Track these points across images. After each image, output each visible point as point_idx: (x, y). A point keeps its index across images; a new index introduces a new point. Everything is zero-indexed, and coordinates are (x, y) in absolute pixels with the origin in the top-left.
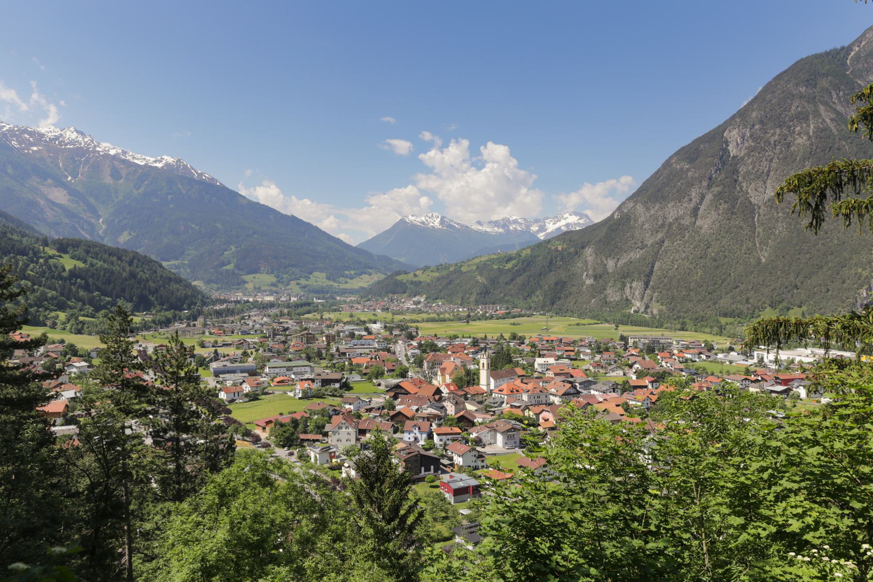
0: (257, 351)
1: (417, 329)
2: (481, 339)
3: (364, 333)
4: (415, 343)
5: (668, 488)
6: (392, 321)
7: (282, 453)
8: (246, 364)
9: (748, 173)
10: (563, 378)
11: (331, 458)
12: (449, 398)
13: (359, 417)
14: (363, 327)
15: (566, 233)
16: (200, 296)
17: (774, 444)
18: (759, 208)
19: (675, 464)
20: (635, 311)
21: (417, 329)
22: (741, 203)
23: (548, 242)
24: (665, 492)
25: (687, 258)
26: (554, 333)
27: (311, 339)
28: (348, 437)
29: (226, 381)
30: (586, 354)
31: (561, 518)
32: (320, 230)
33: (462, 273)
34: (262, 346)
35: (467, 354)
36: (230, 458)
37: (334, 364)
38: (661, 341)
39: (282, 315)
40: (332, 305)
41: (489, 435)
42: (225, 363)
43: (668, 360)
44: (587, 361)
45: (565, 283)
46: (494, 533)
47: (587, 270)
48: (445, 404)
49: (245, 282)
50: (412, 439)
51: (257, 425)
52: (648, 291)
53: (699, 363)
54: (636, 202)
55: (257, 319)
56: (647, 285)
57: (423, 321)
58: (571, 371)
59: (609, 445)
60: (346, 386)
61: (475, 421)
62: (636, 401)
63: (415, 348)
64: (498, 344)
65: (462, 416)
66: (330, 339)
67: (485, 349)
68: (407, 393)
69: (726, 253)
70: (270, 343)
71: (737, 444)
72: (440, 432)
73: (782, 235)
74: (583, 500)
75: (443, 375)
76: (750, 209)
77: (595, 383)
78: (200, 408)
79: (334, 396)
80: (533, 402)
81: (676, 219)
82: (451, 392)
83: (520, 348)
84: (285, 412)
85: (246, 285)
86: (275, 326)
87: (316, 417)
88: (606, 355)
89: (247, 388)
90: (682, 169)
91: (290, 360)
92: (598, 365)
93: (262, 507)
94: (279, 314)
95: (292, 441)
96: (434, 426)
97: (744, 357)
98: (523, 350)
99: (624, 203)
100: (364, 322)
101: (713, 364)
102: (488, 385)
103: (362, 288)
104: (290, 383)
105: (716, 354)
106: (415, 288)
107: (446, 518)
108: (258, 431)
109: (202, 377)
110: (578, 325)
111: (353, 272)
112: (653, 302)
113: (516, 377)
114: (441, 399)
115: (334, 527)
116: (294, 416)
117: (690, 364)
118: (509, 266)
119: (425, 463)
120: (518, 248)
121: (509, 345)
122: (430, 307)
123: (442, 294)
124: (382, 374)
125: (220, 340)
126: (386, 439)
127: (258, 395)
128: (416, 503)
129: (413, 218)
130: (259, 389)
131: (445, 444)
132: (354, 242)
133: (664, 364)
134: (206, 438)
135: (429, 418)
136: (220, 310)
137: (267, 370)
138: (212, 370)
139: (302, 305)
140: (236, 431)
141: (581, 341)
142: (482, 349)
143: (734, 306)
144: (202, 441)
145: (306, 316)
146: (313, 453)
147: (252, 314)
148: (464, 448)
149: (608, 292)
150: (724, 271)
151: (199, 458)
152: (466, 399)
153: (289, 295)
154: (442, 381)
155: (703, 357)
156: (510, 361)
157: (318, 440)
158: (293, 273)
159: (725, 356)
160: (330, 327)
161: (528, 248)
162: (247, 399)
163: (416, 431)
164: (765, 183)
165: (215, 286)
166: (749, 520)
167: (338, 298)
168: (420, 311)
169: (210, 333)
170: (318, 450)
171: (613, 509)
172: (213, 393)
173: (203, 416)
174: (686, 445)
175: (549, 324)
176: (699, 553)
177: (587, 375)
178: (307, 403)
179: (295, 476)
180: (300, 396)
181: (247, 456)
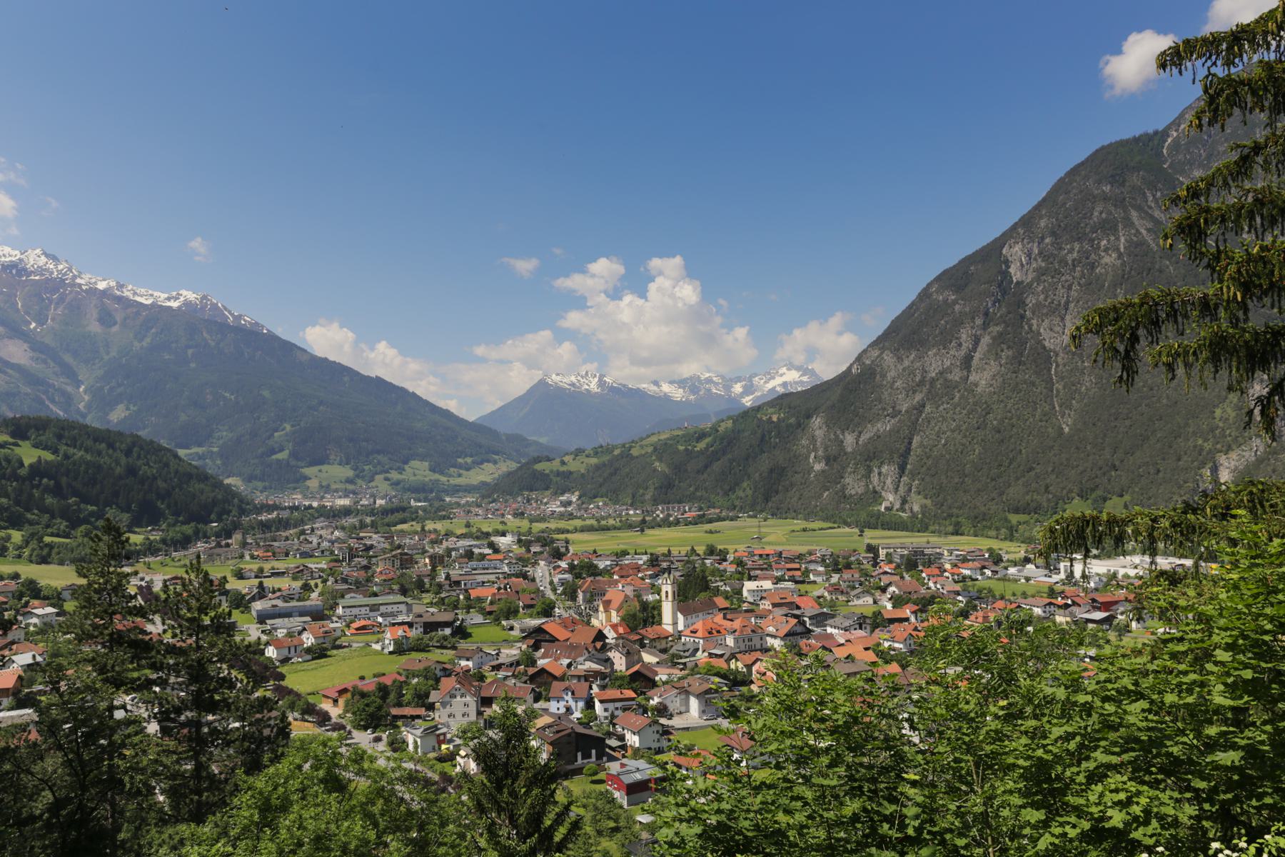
0: (325, 581)
1: (567, 542)
2: (663, 555)
3: (487, 551)
4: (564, 564)
7: (363, 738)
8: (308, 603)
9: (1038, 305)
10: (785, 610)
11: (440, 743)
12: (617, 645)
13: (481, 678)
14: (485, 542)
16: (236, 500)
17: (1082, 698)
18: (1057, 355)
23: (757, 409)
25: (958, 428)
26: (769, 543)
28: (466, 709)
29: (276, 629)
30: (818, 574)
33: (633, 458)
34: (332, 575)
35: (643, 579)
37: (443, 599)
38: (927, 552)
39: (363, 526)
40: (438, 510)
42: (274, 602)
47: (815, 450)
49: (306, 478)
50: (563, 710)
51: (325, 696)
52: (905, 479)
53: (982, 582)
54: (883, 350)
55: (323, 534)
56: (902, 469)
57: (576, 530)
58: (796, 599)
59: (842, 709)
60: (462, 632)
61: (657, 678)
63: (565, 571)
64: (688, 562)
66: (437, 561)
67: (669, 570)
68: (554, 640)
70: (345, 569)
71: (1030, 701)
73: (1091, 393)
74: (809, 795)
75: (606, 611)
76: (1043, 357)
77: (833, 616)
78: (234, 673)
80: (743, 648)
81: (941, 373)
82: (620, 637)
83: (721, 567)
85: (308, 483)
86: (353, 543)
87: (416, 680)
88: (847, 575)
89: (308, 640)
90: (945, 301)
91: (375, 595)
92: (835, 589)
93: (328, 823)
96: (595, 689)
97: (1046, 572)
99: (865, 351)
100: (488, 535)
101: (1001, 583)
102: (675, 624)
103: (484, 483)
105: (1006, 568)
106: (561, 483)
107: (616, 830)
108: (326, 706)
110: (804, 530)
111: (469, 460)
112: (912, 495)
114: (605, 648)
116: (381, 680)
117: (970, 583)
118: (701, 446)
119: (582, 745)
120: (714, 420)
121: (704, 564)
123: (604, 490)
126: (520, 710)
127: (326, 649)
128: (567, 808)
129: (559, 378)
130: (327, 640)
131: (613, 716)
132: (470, 414)
133: (931, 584)
134: (242, 719)
135: (588, 677)
137: (340, 611)
138: (254, 613)
139: (393, 511)
140: (292, 707)
142: (663, 571)
143: (1028, 498)
144: (237, 725)
145: (400, 527)
148: (641, 721)
149: (847, 480)
152: (643, 646)
153: (374, 496)
154: (605, 621)
155: (988, 572)
156: (706, 587)
157: (418, 717)
158: (379, 463)
159: (1019, 571)
161: (729, 418)
162: (309, 657)
163: (569, 697)
164: (1063, 319)
165: (260, 484)
166: (1053, 813)
167: (448, 499)
168: (571, 516)
169: (252, 557)
170: (418, 732)
171: (852, 807)
175: (763, 530)
177: (820, 604)
179: (382, 774)
180: (391, 649)
181: (304, 745)
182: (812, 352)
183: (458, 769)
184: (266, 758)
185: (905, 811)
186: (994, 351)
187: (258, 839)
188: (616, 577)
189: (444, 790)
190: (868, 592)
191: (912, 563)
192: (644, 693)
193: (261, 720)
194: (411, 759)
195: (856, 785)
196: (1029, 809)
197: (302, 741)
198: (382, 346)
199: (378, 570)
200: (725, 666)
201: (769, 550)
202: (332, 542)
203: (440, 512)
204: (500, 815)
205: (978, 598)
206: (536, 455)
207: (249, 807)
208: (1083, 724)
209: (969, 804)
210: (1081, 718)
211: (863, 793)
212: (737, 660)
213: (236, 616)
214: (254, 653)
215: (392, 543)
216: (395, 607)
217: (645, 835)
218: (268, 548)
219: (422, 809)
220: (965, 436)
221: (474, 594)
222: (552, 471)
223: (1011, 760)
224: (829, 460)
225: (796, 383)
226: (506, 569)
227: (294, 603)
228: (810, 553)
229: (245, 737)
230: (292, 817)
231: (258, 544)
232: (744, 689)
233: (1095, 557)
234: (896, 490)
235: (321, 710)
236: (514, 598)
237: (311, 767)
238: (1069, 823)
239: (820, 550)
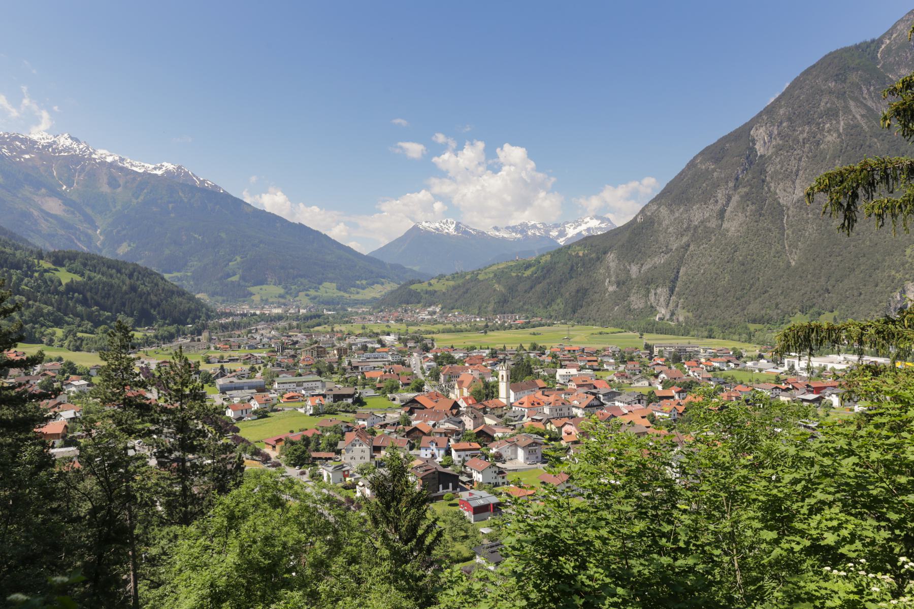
0: (265, 366)
2: (500, 350)
4: (430, 356)
6: (407, 333)
9: (776, 172)
10: (585, 389)
11: (345, 476)
12: (467, 412)
13: (373, 433)
14: (376, 339)
17: (807, 454)
18: (788, 209)
20: (660, 319)
21: (433, 340)
23: (568, 247)
24: (694, 506)
26: (575, 342)
27: (321, 352)
28: (363, 454)
29: (233, 398)
30: (609, 364)
33: (479, 281)
35: (485, 366)
37: (346, 379)
38: (688, 349)
39: (291, 328)
40: (343, 317)
42: (231, 379)
43: (695, 369)
44: (611, 371)
45: (586, 290)
47: (609, 276)
49: (252, 294)
50: (429, 456)
52: (673, 298)
53: (727, 372)
54: (660, 205)
55: (265, 333)
56: (672, 291)
57: (439, 332)
58: (594, 382)
59: (635, 459)
60: (359, 402)
62: (662, 412)
63: (431, 360)
64: (518, 355)
66: (342, 352)
67: (504, 360)
68: (423, 408)
69: (755, 257)
70: (279, 357)
74: (610, 517)
75: (460, 388)
76: (778, 211)
77: (619, 394)
78: (206, 427)
79: (346, 412)
80: (555, 415)
82: (469, 406)
83: (541, 359)
85: (253, 297)
87: (328, 434)
88: (630, 365)
89: (255, 405)
90: (707, 170)
91: (300, 375)
92: (622, 375)
95: (304, 459)
96: (452, 442)
97: (775, 365)
98: (544, 361)
99: (647, 206)
100: (377, 334)
102: (508, 398)
103: (374, 298)
104: (301, 399)
105: (745, 362)
106: (430, 298)
107: (466, 537)
108: (268, 450)
109: (207, 394)
111: (364, 282)
112: (679, 309)
114: (458, 414)
115: (349, 549)
116: (305, 433)
117: (718, 372)
118: (528, 273)
119: (443, 480)
120: (537, 255)
121: (529, 356)
124: (397, 388)
125: (226, 355)
126: (402, 456)
127: (267, 412)
128: (434, 523)
129: (427, 225)
131: (464, 461)
132: (365, 250)
133: (691, 373)
134: (213, 458)
135: (447, 434)
137: (276, 386)
138: (218, 387)
139: (311, 317)
140: (245, 450)
141: (605, 350)
143: (763, 312)
144: (209, 461)
145: (316, 328)
146: (326, 472)
148: (484, 464)
149: (632, 298)
150: (752, 275)
151: (206, 479)
152: (485, 413)
153: (298, 307)
154: (460, 395)
155: (732, 365)
156: (530, 373)
157: (330, 459)
158: (302, 284)
161: (548, 253)
162: (256, 417)
163: (434, 447)
164: (794, 183)
165: (220, 298)
166: (782, 535)
167: (349, 309)
168: (435, 322)
169: (216, 348)
170: (330, 469)
173: (210, 435)
174: (716, 457)
175: (571, 333)
177: (610, 386)
178: (318, 420)
183: (358, 494)
188: (467, 365)
189: (349, 509)
201: (575, 347)
206: (411, 279)
208: (807, 472)
220: (718, 268)
230: (249, 523)
234: (667, 305)
236: (395, 378)
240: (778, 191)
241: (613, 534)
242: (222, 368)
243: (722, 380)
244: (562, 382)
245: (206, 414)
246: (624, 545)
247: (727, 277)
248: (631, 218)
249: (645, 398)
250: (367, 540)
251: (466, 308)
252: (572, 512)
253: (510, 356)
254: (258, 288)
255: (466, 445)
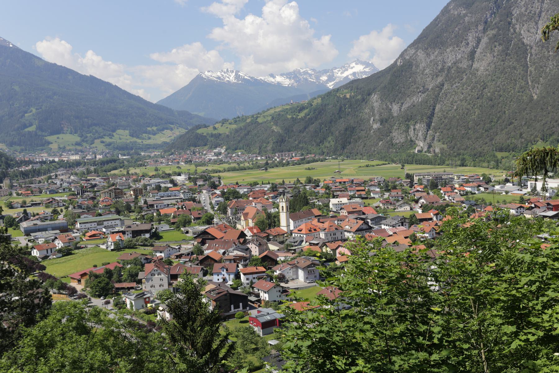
0: (67, 208)
1: (220, 178)
2: (280, 184)
3: (170, 185)
4: (218, 192)
5: (449, 306)
6: (196, 173)
7: (98, 302)
8: (56, 222)
9: (521, 15)
10: (356, 216)
11: (146, 303)
12: (253, 240)
13: (170, 263)
14: (168, 180)
15: (353, 82)
16: (3, 158)
17: (540, 260)
18: (531, 48)
19: (455, 283)
20: (419, 151)
21: (220, 178)
22: (514, 44)
23: (337, 90)
24: (447, 309)
25: (465, 99)
26: (346, 175)
27: (119, 193)
28: (161, 282)
29: (37, 239)
30: (376, 193)
31: (354, 338)
32: (120, 89)
33: (259, 124)
34: (72, 203)
35: (267, 199)
36: (46, 312)
37: (143, 216)
38: (444, 177)
39: (89, 172)
40: (137, 160)
41: (291, 271)
42: (35, 222)
43: (449, 194)
44: (377, 199)
45: (354, 128)
46: (294, 355)
47: (374, 115)
48: (249, 246)
49: (49, 143)
50: (221, 280)
51: (72, 278)
52: (430, 132)
53: (478, 195)
54: (417, 49)
55: (63, 178)
56: (429, 126)
57: (225, 171)
58: (363, 209)
59: (396, 270)
60: (156, 236)
61: (278, 259)
62: (424, 232)
63: (219, 196)
64: (295, 188)
65: (266, 256)
66: (138, 193)
67: (283, 193)
68: (214, 238)
69: (501, 93)
70: (79, 200)
71: (508, 263)
72: (246, 272)
73: (553, 73)
74: (374, 321)
75: (246, 219)
76: (522, 50)
77: (385, 218)
78: (12, 266)
79: (145, 245)
80: (330, 239)
81: (455, 63)
82: (254, 235)
83: (316, 190)
84: (99, 263)
85: (51, 146)
86: (83, 183)
87: (129, 266)
88: (394, 193)
89: (59, 244)
90: (459, 15)
91: (100, 215)
92: (387, 202)
93: (80, 353)
94: (85, 171)
95: (108, 290)
96: (241, 267)
97: (519, 188)
98: (318, 193)
99: (406, 50)
100: (169, 175)
101: (491, 195)
102: (288, 226)
103: (165, 143)
104: (102, 236)
105: (494, 186)
106: (215, 141)
107: (256, 349)
108: (74, 284)
109: (12, 237)
110: (367, 166)
111: (155, 128)
112: (435, 142)
113: (313, 217)
114: (245, 242)
115: (151, 365)
116: (108, 267)
117: (470, 196)
118: (302, 115)
119: (234, 301)
120: (309, 98)
121: (305, 189)
122: (231, 158)
123: (241, 145)
124: (189, 222)
125: (28, 200)
126: (195, 281)
127: (71, 250)
128: (226, 338)
129: (210, 74)
130: (71, 244)
131: (252, 283)
132: (154, 99)
133: (446, 197)
134: (20, 294)
135: (236, 260)
136: (26, 171)
137: (78, 226)
138: (22, 230)
139: (108, 162)
140: (52, 286)
141: (371, 181)
142: (280, 194)
143: (509, 142)
144: (17, 298)
145: (113, 172)
146: (129, 300)
147: (59, 173)
148: (269, 285)
149: (394, 134)
150: (499, 109)
151: (15, 314)
152: (269, 240)
153: (95, 153)
154: (245, 225)
155: (482, 189)
156: (307, 203)
157: (132, 288)
158: (97, 132)
159: (501, 187)
160: (137, 181)
161: (319, 97)
162: (61, 255)
163: (224, 272)
164: (537, 24)
165: (18, 148)
166: (520, 328)
167: (143, 154)
168: (221, 162)
169: (18, 194)
170: (133, 297)
171: (399, 329)
172: (26, 252)
173: (16, 274)
174: (464, 266)
175: (341, 167)
176: (478, 361)
177: (377, 211)
178: (118, 255)
179: (112, 322)
180: (112, 248)
181: (61, 307)
182: (373, 52)
183: (159, 318)
184: (38, 315)
185: (432, 329)
186: (490, 47)
187: (37, 364)
188: (251, 199)
189: (150, 331)
190: (406, 203)
191: (434, 184)
192: (271, 268)
193: (32, 294)
194: (129, 313)
195: (403, 314)
196: (506, 326)
197: (61, 305)
198: (90, 54)
199: (101, 199)
200: (319, 250)
201: (345, 179)
202: (70, 183)
203: (139, 162)
204: (185, 343)
205: (476, 205)
206: (197, 124)
207: (29, 346)
208: (541, 275)
209: (470, 325)
210: (540, 271)
211: (407, 320)
212: (327, 247)
213: (11, 231)
214: (25, 253)
215: (109, 182)
216: (110, 222)
217: (274, 352)
218: (28, 188)
219: (138, 342)
220: (469, 104)
221: (162, 212)
222: (208, 134)
223: (496, 297)
224: (382, 121)
225: (361, 72)
226: (182, 196)
227: (48, 222)
228: (371, 181)
229: (23, 305)
230: (57, 350)
231: (21, 186)
232: (331, 264)
233: (550, 177)
234: (425, 139)
235: (71, 286)
236: (188, 213)
237: (67, 320)
238: (530, 333)
239: (378, 178)
240: (522, 32)
241: (377, 335)
242: (25, 212)
243: (474, 203)
244: (334, 210)
245: (12, 255)
246: (387, 345)
247: (477, 112)
248: (392, 62)
249: (407, 221)
250: (167, 357)
251: (248, 148)
252: (342, 318)
253: (288, 190)
254: (55, 136)
255: (252, 269)
